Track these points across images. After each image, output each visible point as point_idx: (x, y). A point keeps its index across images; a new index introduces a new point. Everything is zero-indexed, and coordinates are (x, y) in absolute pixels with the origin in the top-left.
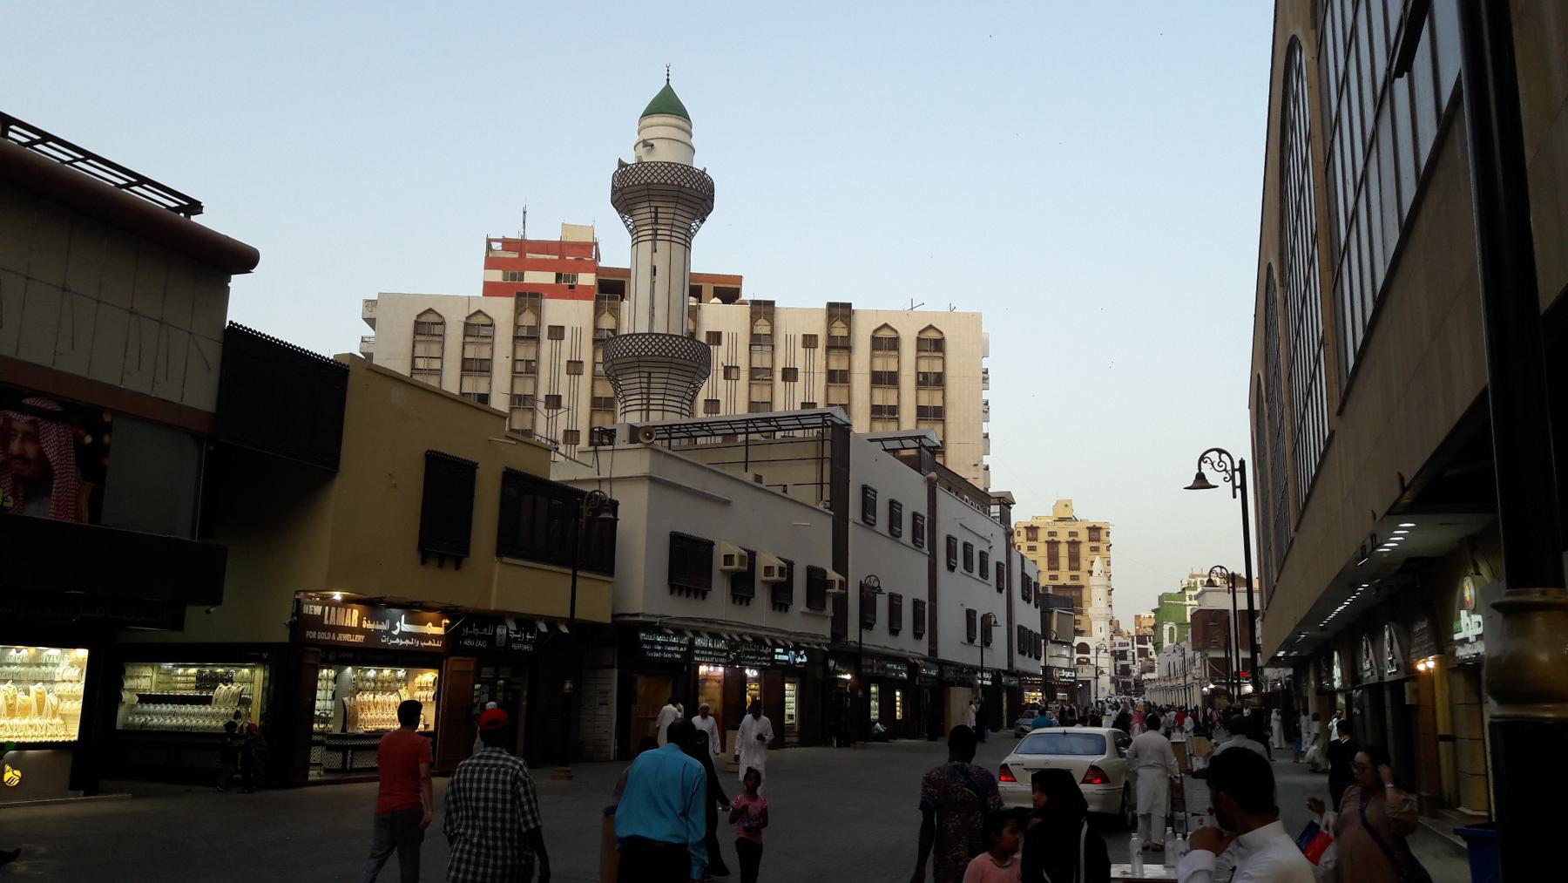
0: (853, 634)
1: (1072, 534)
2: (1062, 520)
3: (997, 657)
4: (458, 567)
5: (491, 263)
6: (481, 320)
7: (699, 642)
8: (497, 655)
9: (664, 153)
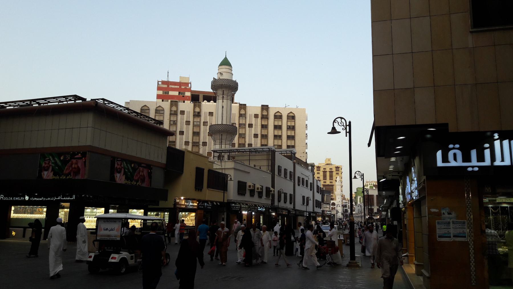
0: (276, 203)
1: (331, 169)
2: (327, 164)
3: (310, 208)
4: (201, 191)
5: (159, 89)
6: (160, 108)
7: (242, 206)
8: (205, 209)
9: (225, 76)
